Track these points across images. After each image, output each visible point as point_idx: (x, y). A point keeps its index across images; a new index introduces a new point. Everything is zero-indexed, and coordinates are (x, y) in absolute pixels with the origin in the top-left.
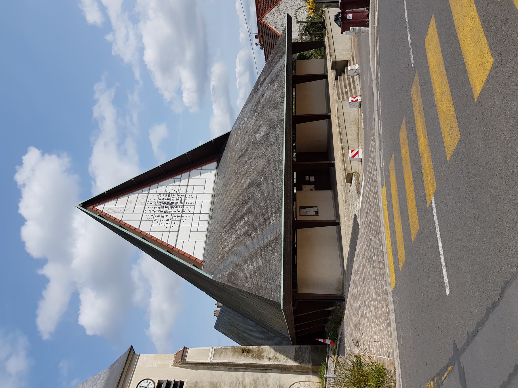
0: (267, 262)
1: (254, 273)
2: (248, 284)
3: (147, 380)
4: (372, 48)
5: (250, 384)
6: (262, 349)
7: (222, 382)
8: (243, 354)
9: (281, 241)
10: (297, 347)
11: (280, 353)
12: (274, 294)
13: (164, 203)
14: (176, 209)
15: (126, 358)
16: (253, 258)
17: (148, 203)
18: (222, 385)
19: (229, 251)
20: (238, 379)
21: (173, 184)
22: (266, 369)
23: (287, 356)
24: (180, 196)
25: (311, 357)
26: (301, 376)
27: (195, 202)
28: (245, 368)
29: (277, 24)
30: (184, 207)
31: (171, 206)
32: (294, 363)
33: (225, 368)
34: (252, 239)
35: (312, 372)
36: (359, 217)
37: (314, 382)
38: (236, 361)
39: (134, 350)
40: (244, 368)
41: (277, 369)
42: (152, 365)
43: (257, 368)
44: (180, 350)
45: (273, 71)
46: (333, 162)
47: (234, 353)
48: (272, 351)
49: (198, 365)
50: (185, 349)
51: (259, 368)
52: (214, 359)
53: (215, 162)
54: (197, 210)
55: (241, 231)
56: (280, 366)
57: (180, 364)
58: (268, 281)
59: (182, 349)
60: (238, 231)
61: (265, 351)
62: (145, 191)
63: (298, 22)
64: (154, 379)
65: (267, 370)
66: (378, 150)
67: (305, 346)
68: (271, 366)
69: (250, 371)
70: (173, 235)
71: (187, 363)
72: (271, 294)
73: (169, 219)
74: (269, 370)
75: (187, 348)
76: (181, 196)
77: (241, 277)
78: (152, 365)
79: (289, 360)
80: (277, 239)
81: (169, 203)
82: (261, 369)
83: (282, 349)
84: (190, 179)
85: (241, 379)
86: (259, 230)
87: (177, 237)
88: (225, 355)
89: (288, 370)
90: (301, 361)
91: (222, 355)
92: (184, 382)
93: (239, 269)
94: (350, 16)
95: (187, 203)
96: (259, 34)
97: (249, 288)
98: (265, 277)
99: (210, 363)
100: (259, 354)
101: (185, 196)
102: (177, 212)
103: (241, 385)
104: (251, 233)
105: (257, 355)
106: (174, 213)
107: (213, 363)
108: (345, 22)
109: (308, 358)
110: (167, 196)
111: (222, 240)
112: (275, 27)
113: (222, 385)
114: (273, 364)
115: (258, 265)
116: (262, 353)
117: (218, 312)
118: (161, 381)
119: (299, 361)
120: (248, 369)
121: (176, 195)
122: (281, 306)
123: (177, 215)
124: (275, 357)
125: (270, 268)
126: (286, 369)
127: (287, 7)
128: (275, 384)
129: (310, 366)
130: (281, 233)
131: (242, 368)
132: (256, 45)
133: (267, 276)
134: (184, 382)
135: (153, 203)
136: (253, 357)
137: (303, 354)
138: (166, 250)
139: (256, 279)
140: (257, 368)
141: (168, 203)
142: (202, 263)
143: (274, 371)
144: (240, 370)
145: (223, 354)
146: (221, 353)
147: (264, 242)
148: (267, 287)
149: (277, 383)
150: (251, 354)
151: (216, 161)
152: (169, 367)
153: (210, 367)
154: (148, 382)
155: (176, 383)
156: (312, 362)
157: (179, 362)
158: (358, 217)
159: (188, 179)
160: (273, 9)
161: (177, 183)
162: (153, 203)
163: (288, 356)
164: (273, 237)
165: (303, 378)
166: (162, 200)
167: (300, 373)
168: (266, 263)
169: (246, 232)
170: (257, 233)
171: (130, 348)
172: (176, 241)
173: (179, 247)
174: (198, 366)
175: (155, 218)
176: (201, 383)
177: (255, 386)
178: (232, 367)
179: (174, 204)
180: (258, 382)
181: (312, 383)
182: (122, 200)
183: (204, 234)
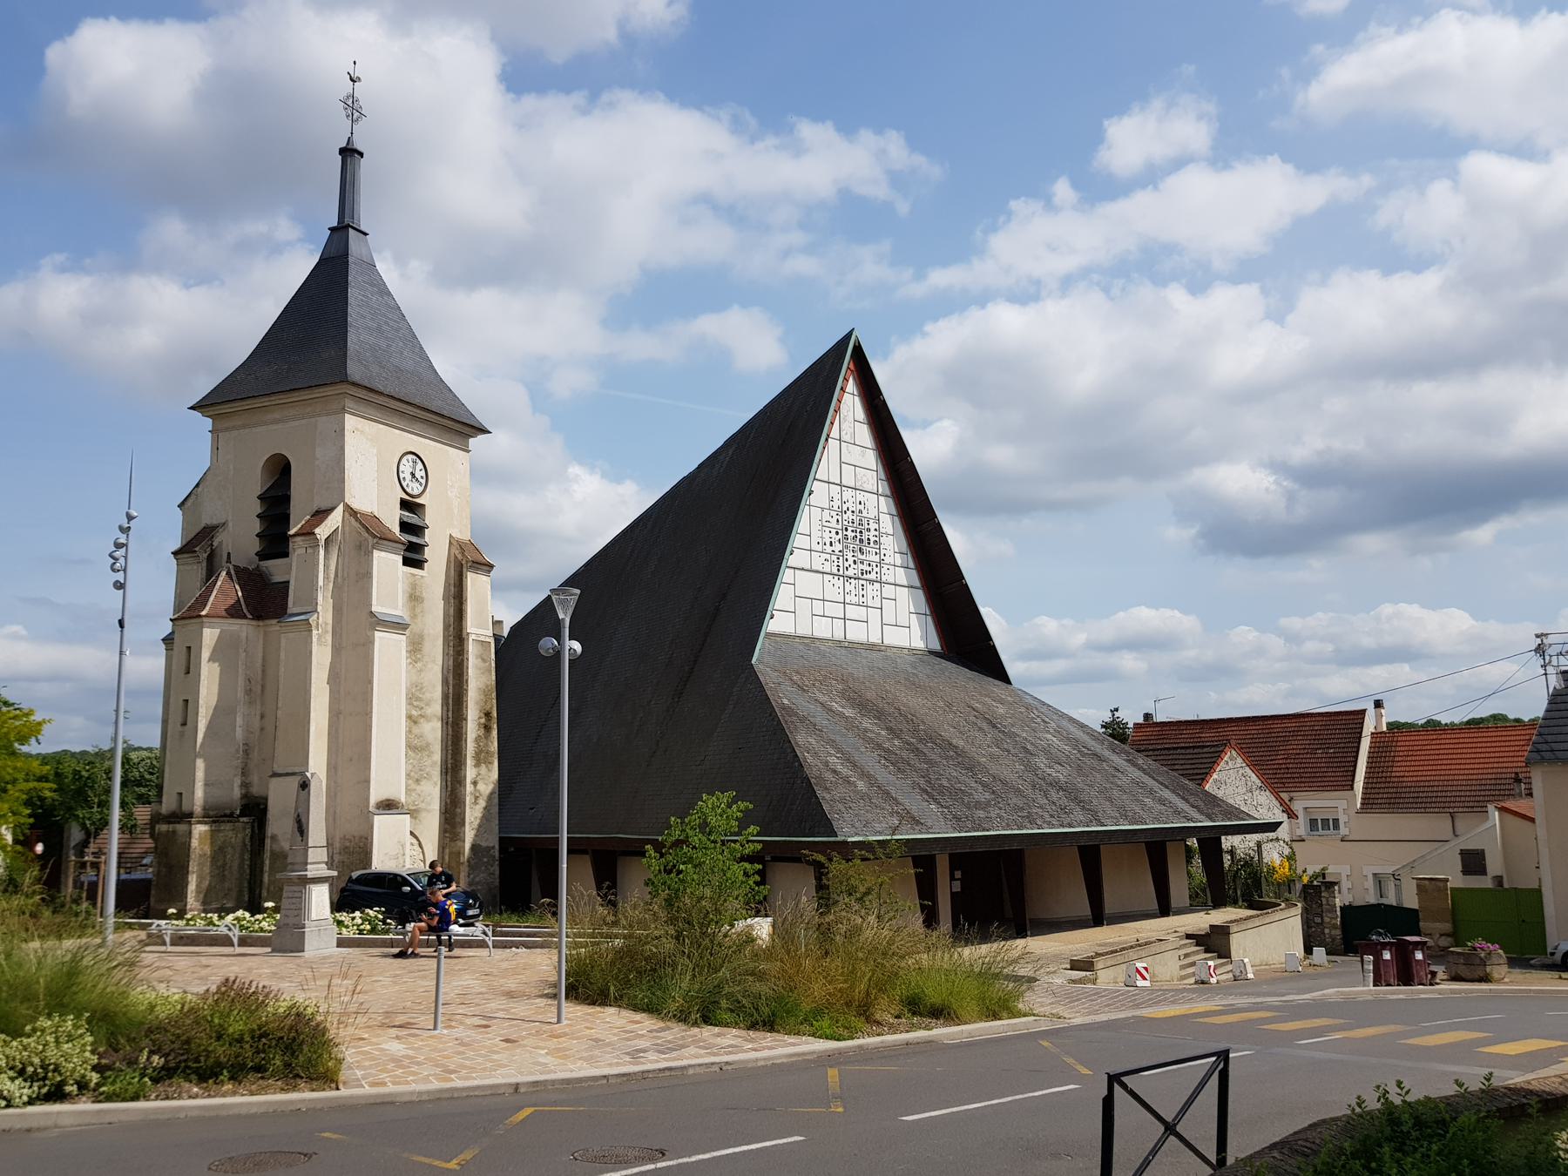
4: (1353, 991)
5: (421, 736)
11: (485, 808)
13: (861, 532)
14: (851, 560)
17: (860, 496)
21: (897, 550)
23: (480, 826)
24: (876, 569)
27: (865, 604)
29: (1223, 786)
30: (855, 579)
31: (857, 548)
41: (448, 801)
43: (450, 751)
45: (1167, 791)
46: (1029, 933)
47: (484, 692)
49: (457, 601)
50: (488, 568)
51: (450, 757)
53: (942, 646)
54: (852, 612)
56: (458, 810)
57: (456, 557)
62: (884, 487)
63: (1259, 845)
66: (1223, 1003)
68: (458, 786)
73: (833, 548)
75: (490, 572)
76: (875, 572)
79: (473, 832)
81: (862, 543)
82: (446, 761)
84: (907, 589)
85: (429, 711)
88: (480, 669)
90: (472, 862)
94: (1387, 956)
95: (863, 585)
96: (1157, 723)
101: (877, 582)
102: (846, 564)
103: (420, 713)
106: (845, 557)
107: (466, 642)
108: (1379, 947)
109: (477, 879)
110: (876, 539)
112: (1215, 781)
113: (419, 665)
116: (484, 763)
121: (877, 558)
123: (841, 566)
126: (448, 824)
127: (1260, 810)
128: (422, 799)
132: (1111, 711)
135: (861, 507)
136: (477, 740)
141: (861, 541)
151: (942, 649)
159: (905, 583)
160: (1254, 775)
161: (898, 560)
162: (861, 507)
166: (867, 526)
172: (794, 568)
175: (834, 513)
179: (860, 556)
182: (864, 435)
183: (807, 632)
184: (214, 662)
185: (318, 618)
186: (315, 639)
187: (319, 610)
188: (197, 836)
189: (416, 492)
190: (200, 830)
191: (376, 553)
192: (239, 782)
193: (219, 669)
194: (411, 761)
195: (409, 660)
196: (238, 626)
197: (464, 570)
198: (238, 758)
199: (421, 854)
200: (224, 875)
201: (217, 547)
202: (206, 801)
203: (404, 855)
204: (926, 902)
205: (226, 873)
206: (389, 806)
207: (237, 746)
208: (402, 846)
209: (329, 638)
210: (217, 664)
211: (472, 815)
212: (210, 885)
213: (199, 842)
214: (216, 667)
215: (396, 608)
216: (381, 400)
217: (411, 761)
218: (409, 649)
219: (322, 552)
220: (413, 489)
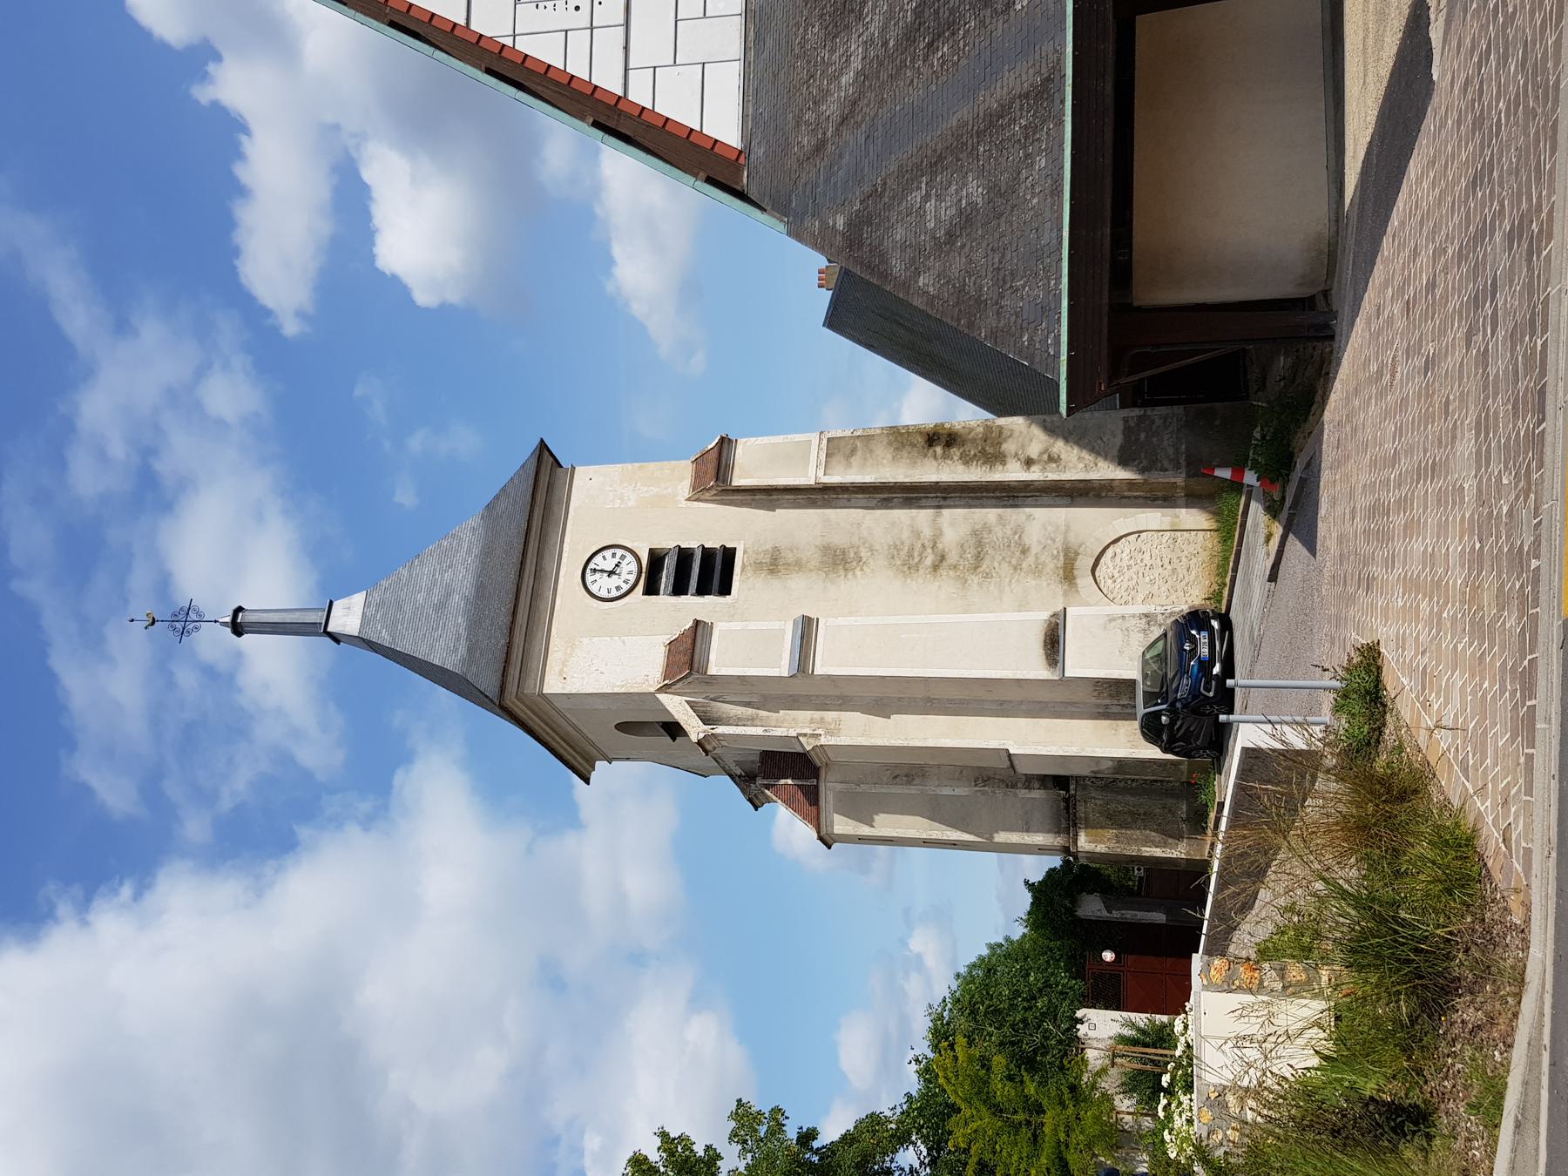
0: (1003, 196)
1: (950, 235)
2: (926, 281)
3: (612, 551)
5: (962, 546)
6: (1001, 428)
7: (864, 543)
8: (931, 451)
9: (1063, 102)
10: (1132, 414)
11: (1066, 440)
12: (1031, 340)
15: (531, 482)
16: (942, 168)
18: (862, 555)
19: (844, 120)
20: (917, 534)
22: (1014, 496)
25: (1183, 447)
26: (1144, 512)
28: (939, 495)
32: (1117, 472)
33: (870, 497)
34: (937, 78)
35: (1186, 496)
36: (1441, 20)
37: (1190, 530)
38: (906, 476)
39: (551, 454)
40: (937, 497)
42: (621, 498)
43: (984, 494)
44: (710, 447)
47: (897, 449)
48: (1034, 435)
49: (774, 493)
50: (725, 445)
52: (827, 472)
55: (884, 29)
58: (1008, 278)
59: (714, 443)
60: (874, 29)
61: (1011, 435)
64: (635, 544)
65: (1018, 497)
67: (1162, 410)
69: (957, 503)
70: (608, 42)
71: (738, 490)
72: (1021, 337)
74: (1028, 497)
77: (898, 245)
78: (621, 498)
79: (1102, 464)
80: (1045, 91)
82: (997, 498)
83: (1075, 427)
85: (927, 532)
86: (961, 32)
87: (626, 48)
88: (865, 459)
89: (1098, 496)
90: (1145, 463)
91: (854, 457)
92: (734, 550)
93: (889, 207)
97: (931, 300)
98: (996, 260)
99: (817, 486)
100: (987, 448)
103: (929, 550)
104: (930, 45)
105: (983, 452)
109: (1171, 451)
111: (809, 62)
113: (864, 553)
114: (1042, 478)
115: (964, 202)
116: (1000, 444)
117: (835, 273)
118: (659, 551)
119: (1138, 464)
120: (952, 497)
122: (1061, 405)
124: (1049, 456)
125: (1015, 225)
129: (1180, 480)
130: (1060, 61)
131: (930, 495)
133: (1003, 256)
134: (734, 550)
136: (966, 460)
137: (1155, 440)
138: (591, 120)
139: (958, 264)
140: (984, 494)
142: (742, 161)
143: (1045, 499)
144: (923, 502)
145: (859, 453)
146: (853, 451)
147: (988, 98)
148: (1002, 307)
149: (1057, 540)
150: (961, 450)
152: (680, 505)
153: (819, 497)
154: (618, 556)
155: (708, 554)
156: (1187, 466)
157: (710, 489)
158: (1432, 17)
163: (1097, 448)
164: (1024, 77)
165: (1153, 518)
167: (1141, 501)
168: (999, 201)
169: (910, 37)
170: (955, 49)
171: (538, 450)
172: (626, 70)
173: (639, 95)
174: (775, 497)
176: (792, 551)
177: (979, 553)
178: (894, 495)
180: (987, 541)
181: (1185, 533)
183: (737, 24)
184: (873, 820)
185: (805, 735)
186: (832, 741)
187: (794, 734)
188: (1093, 845)
189: (634, 567)
190: (1085, 843)
191: (713, 670)
192: (1024, 791)
193: (882, 815)
194: (996, 564)
195: (858, 573)
196: (829, 792)
197: (729, 488)
198: (994, 792)
199: (1129, 538)
200: (1145, 814)
201: (745, 773)
202: (1049, 832)
203: (1123, 617)
204: (1146, 382)
205: (1141, 811)
206: (1053, 642)
207: (979, 794)
208: (1110, 621)
209: (830, 715)
210: (876, 817)
211: (1075, 467)
212: (1156, 831)
213: (1100, 843)
214: (880, 818)
215: (783, 631)
216: (519, 639)
217: (996, 564)
218: (842, 572)
219: (720, 730)
220: (630, 573)
